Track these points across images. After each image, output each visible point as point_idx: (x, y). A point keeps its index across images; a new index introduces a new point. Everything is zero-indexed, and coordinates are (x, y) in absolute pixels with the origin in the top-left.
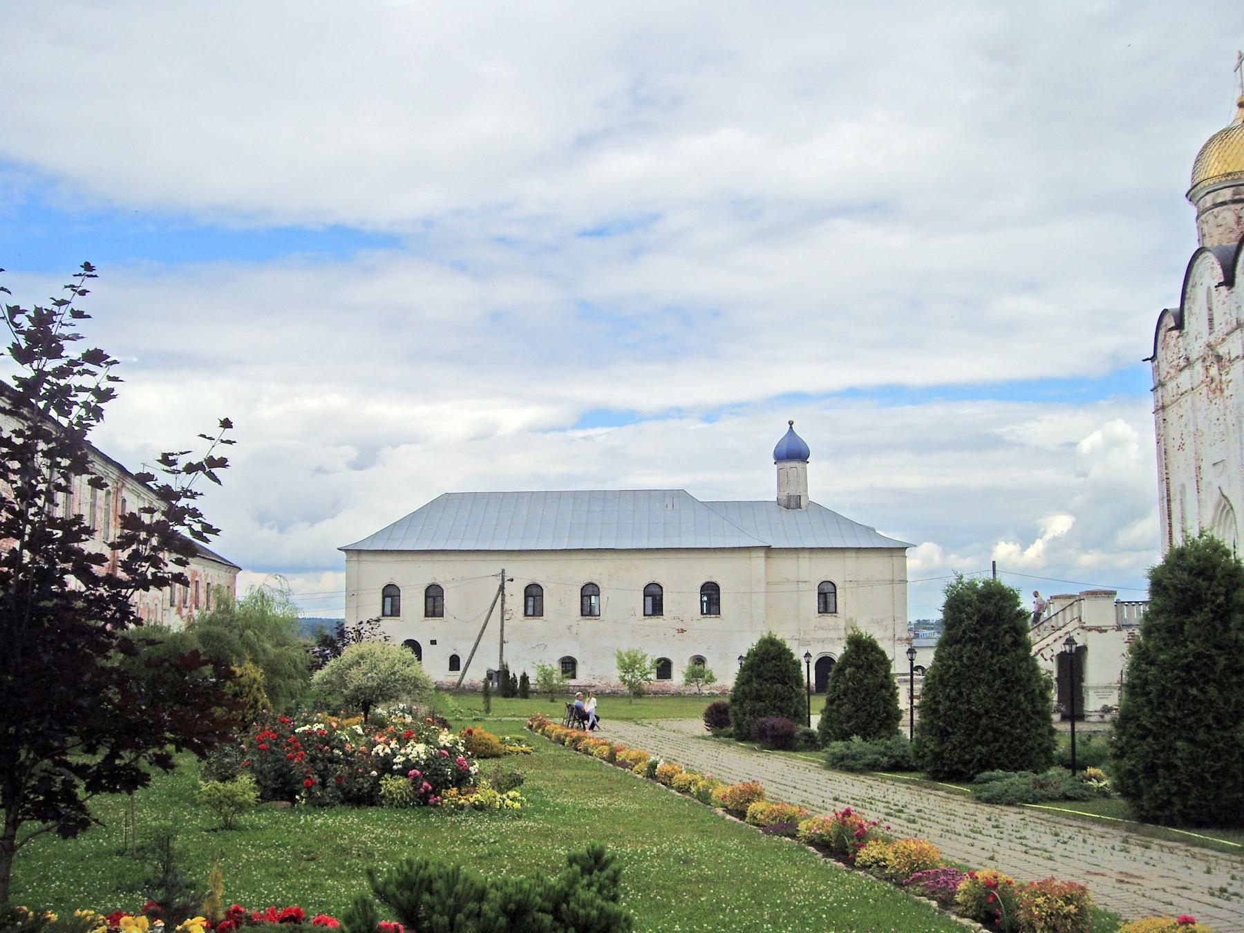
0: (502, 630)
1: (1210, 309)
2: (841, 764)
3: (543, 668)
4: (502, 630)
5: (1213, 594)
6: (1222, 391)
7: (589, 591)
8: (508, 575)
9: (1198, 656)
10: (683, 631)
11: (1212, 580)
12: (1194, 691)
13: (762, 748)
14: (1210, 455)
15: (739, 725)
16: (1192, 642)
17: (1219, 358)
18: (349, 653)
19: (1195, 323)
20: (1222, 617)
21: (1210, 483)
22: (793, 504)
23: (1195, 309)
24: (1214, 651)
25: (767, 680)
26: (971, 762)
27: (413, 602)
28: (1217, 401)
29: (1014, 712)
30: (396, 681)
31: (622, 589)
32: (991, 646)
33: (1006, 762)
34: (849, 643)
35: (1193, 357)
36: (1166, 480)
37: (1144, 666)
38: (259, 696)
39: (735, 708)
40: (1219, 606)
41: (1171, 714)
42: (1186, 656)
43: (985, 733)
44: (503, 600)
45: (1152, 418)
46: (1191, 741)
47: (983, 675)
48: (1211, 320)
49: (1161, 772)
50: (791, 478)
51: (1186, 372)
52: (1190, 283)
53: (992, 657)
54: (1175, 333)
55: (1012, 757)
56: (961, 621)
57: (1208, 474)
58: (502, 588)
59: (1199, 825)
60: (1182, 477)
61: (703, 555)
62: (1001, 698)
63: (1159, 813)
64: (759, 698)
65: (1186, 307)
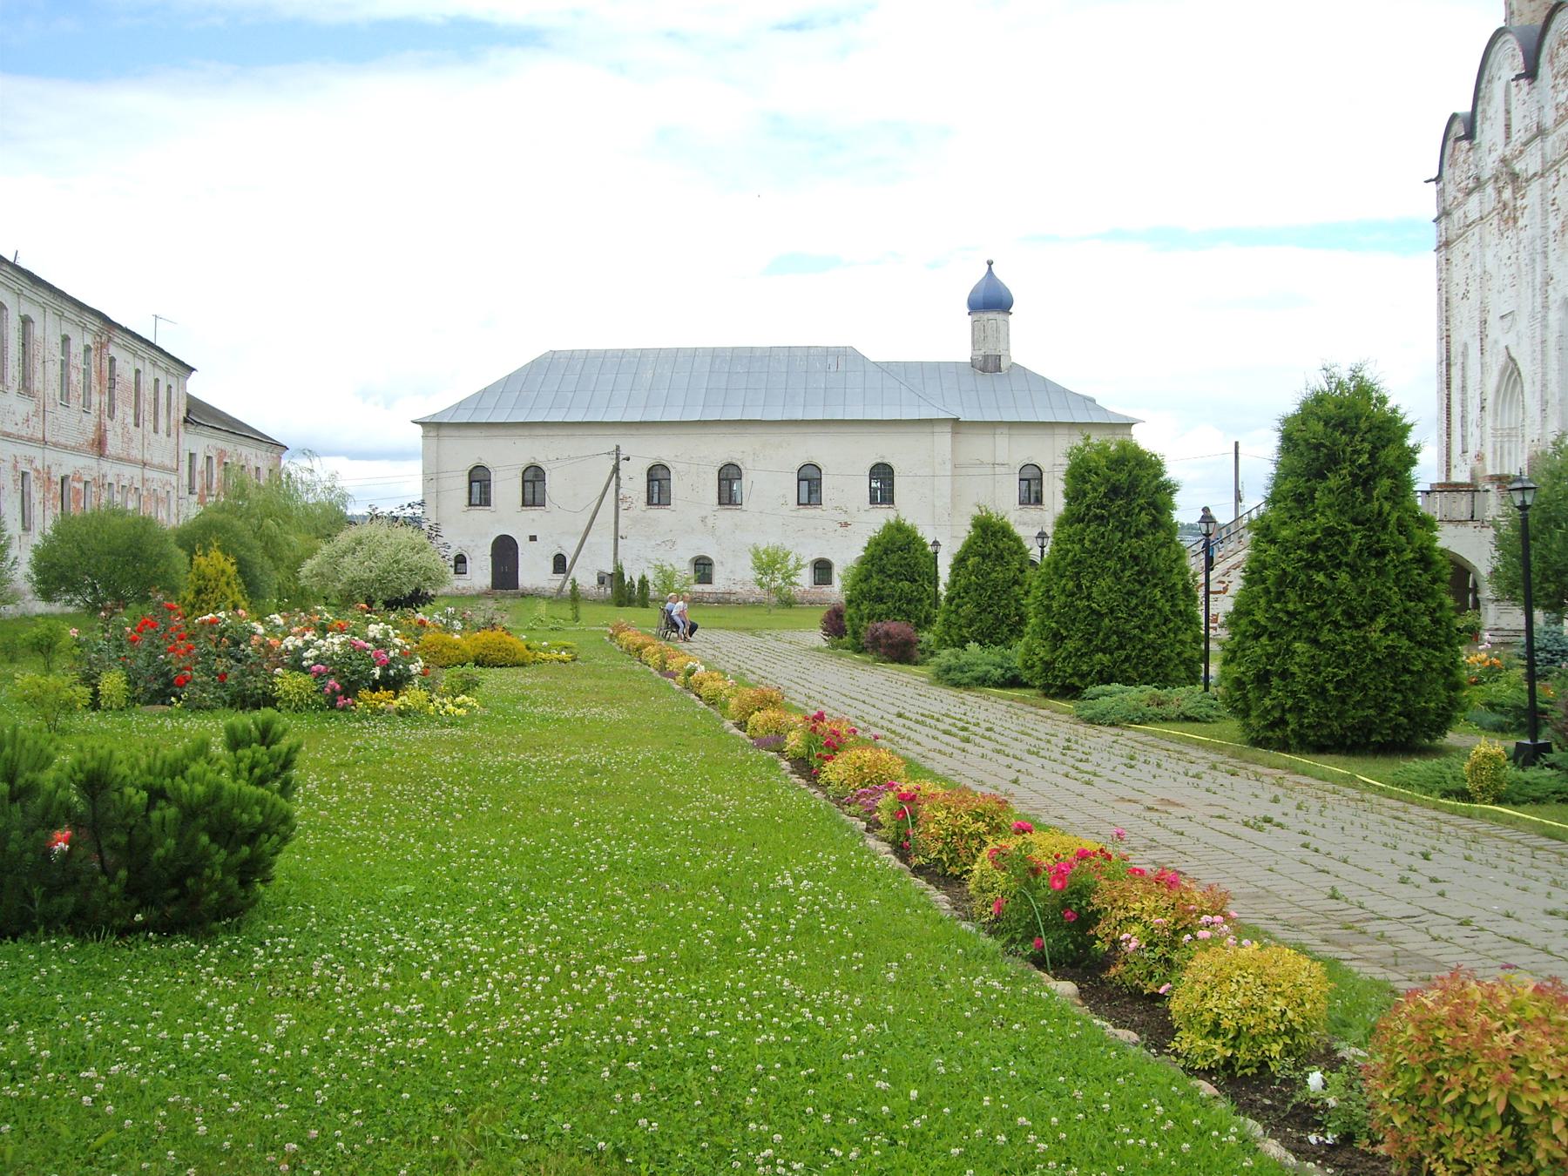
0: (616, 523)
1: (1508, 112)
2: (951, 678)
3: (661, 570)
4: (616, 523)
5: (1354, 452)
6: (1515, 220)
7: (729, 476)
8: (624, 453)
9: (1329, 532)
10: (846, 524)
11: (1354, 434)
12: (1320, 577)
13: (876, 660)
14: (1499, 304)
15: (856, 634)
16: (1322, 514)
17: (1514, 177)
18: (344, 538)
19: (1491, 132)
20: (1365, 483)
21: (1496, 342)
22: (990, 366)
23: (1490, 113)
24: (1350, 526)
25: (890, 576)
26: (1089, 674)
27: (507, 488)
28: (1509, 233)
29: (1146, 612)
30: (400, 571)
31: (770, 472)
32: (1122, 527)
33: (1134, 675)
34: (974, 526)
35: (1486, 175)
36: (1446, 338)
37: (1264, 546)
38: (229, 592)
39: (851, 611)
40: (1361, 467)
41: (1291, 607)
42: (1313, 532)
43: (1107, 637)
44: (618, 485)
45: (1432, 257)
46: (1315, 642)
47: (1108, 563)
48: (1508, 127)
49: (1275, 681)
50: (989, 332)
51: (1475, 197)
52: (1486, 78)
53: (1122, 541)
54: (1465, 144)
55: (1141, 669)
56: (1085, 495)
57: (1495, 329)
58: (616, 469)
59: (1320, 749)
60: (1465, 333)
61: (872, 429)
62: (1130, 593)
63: (1270, 734)
64: (880, 599)
65: (1479, 109)
